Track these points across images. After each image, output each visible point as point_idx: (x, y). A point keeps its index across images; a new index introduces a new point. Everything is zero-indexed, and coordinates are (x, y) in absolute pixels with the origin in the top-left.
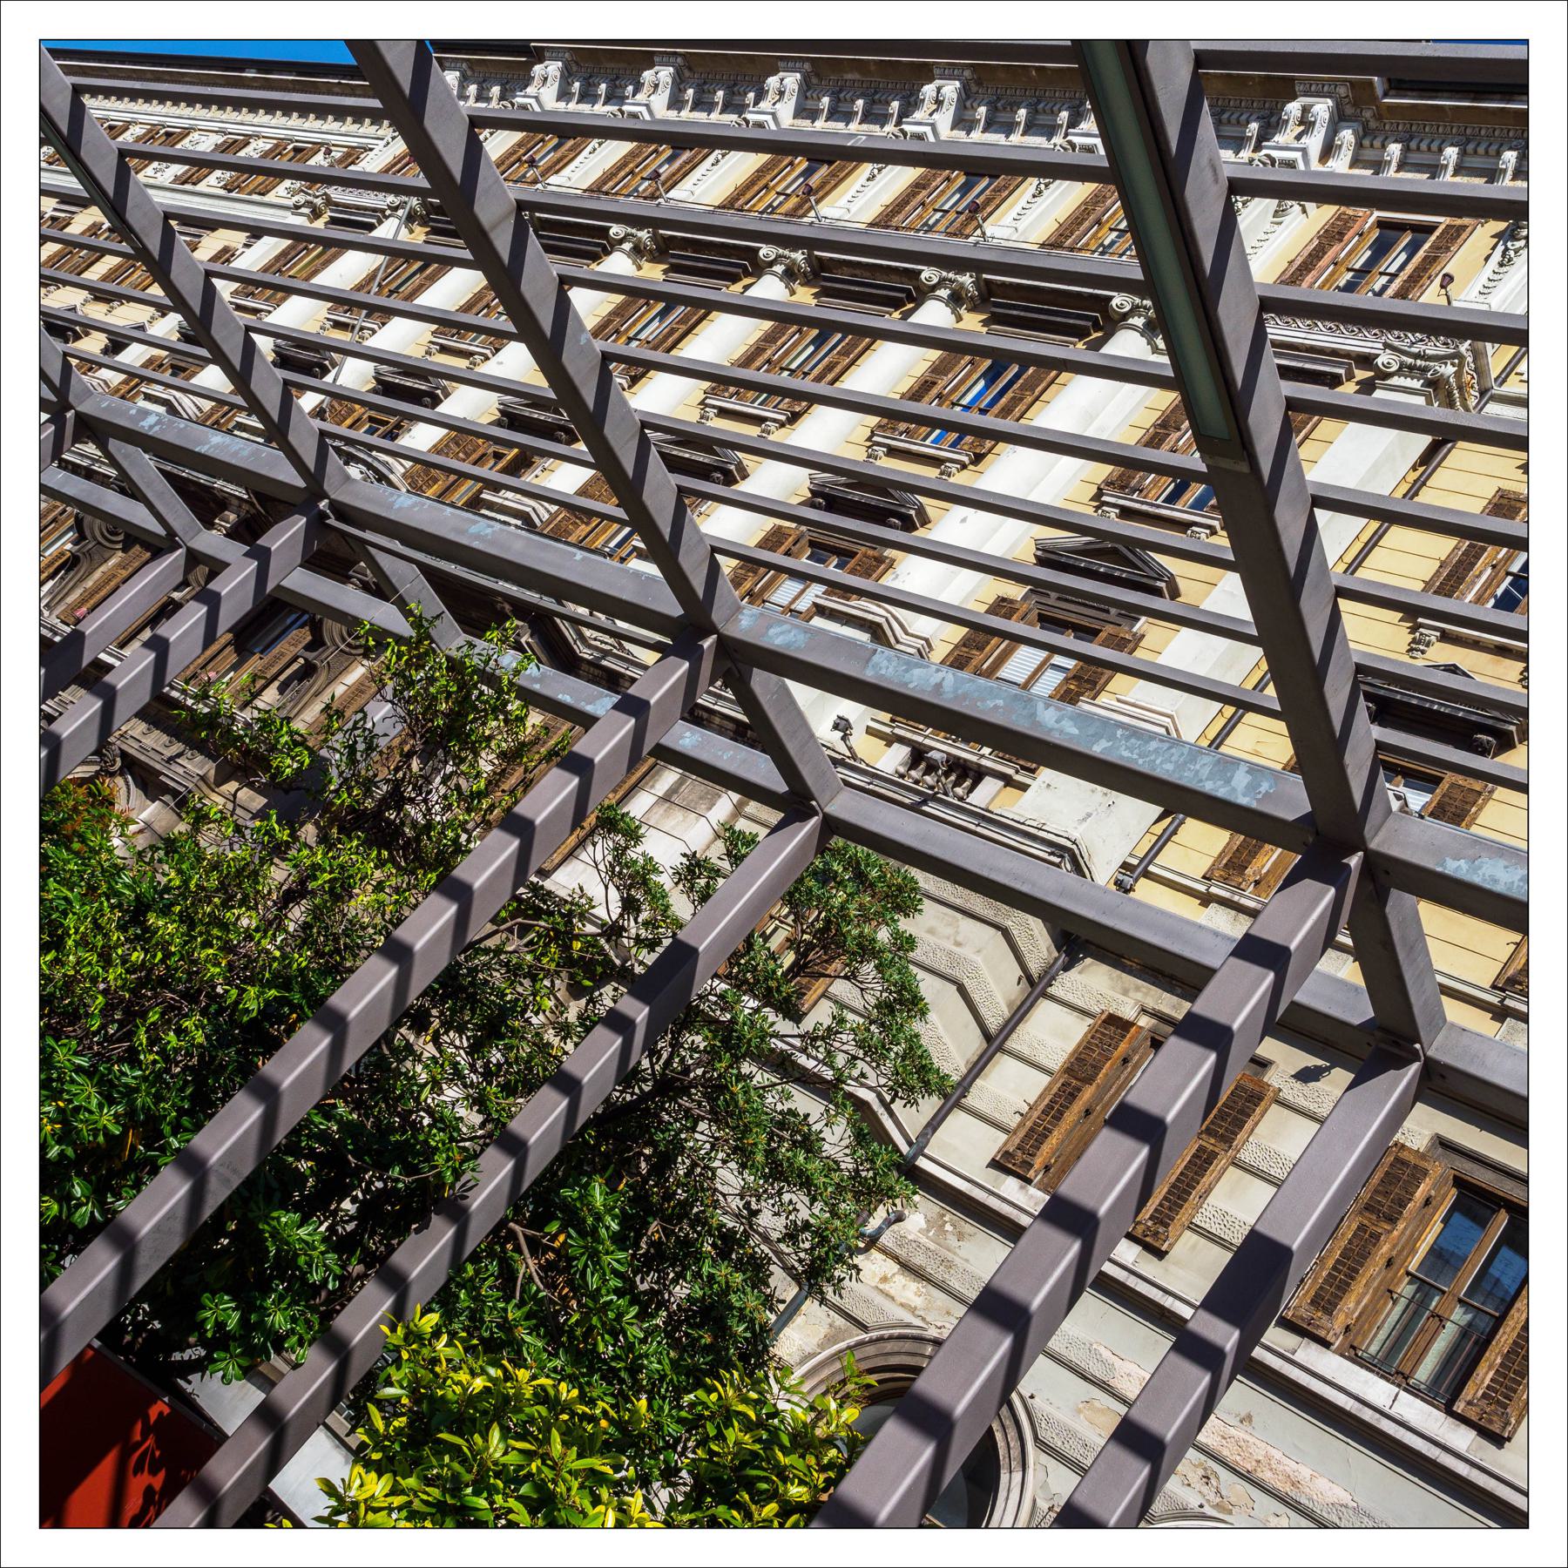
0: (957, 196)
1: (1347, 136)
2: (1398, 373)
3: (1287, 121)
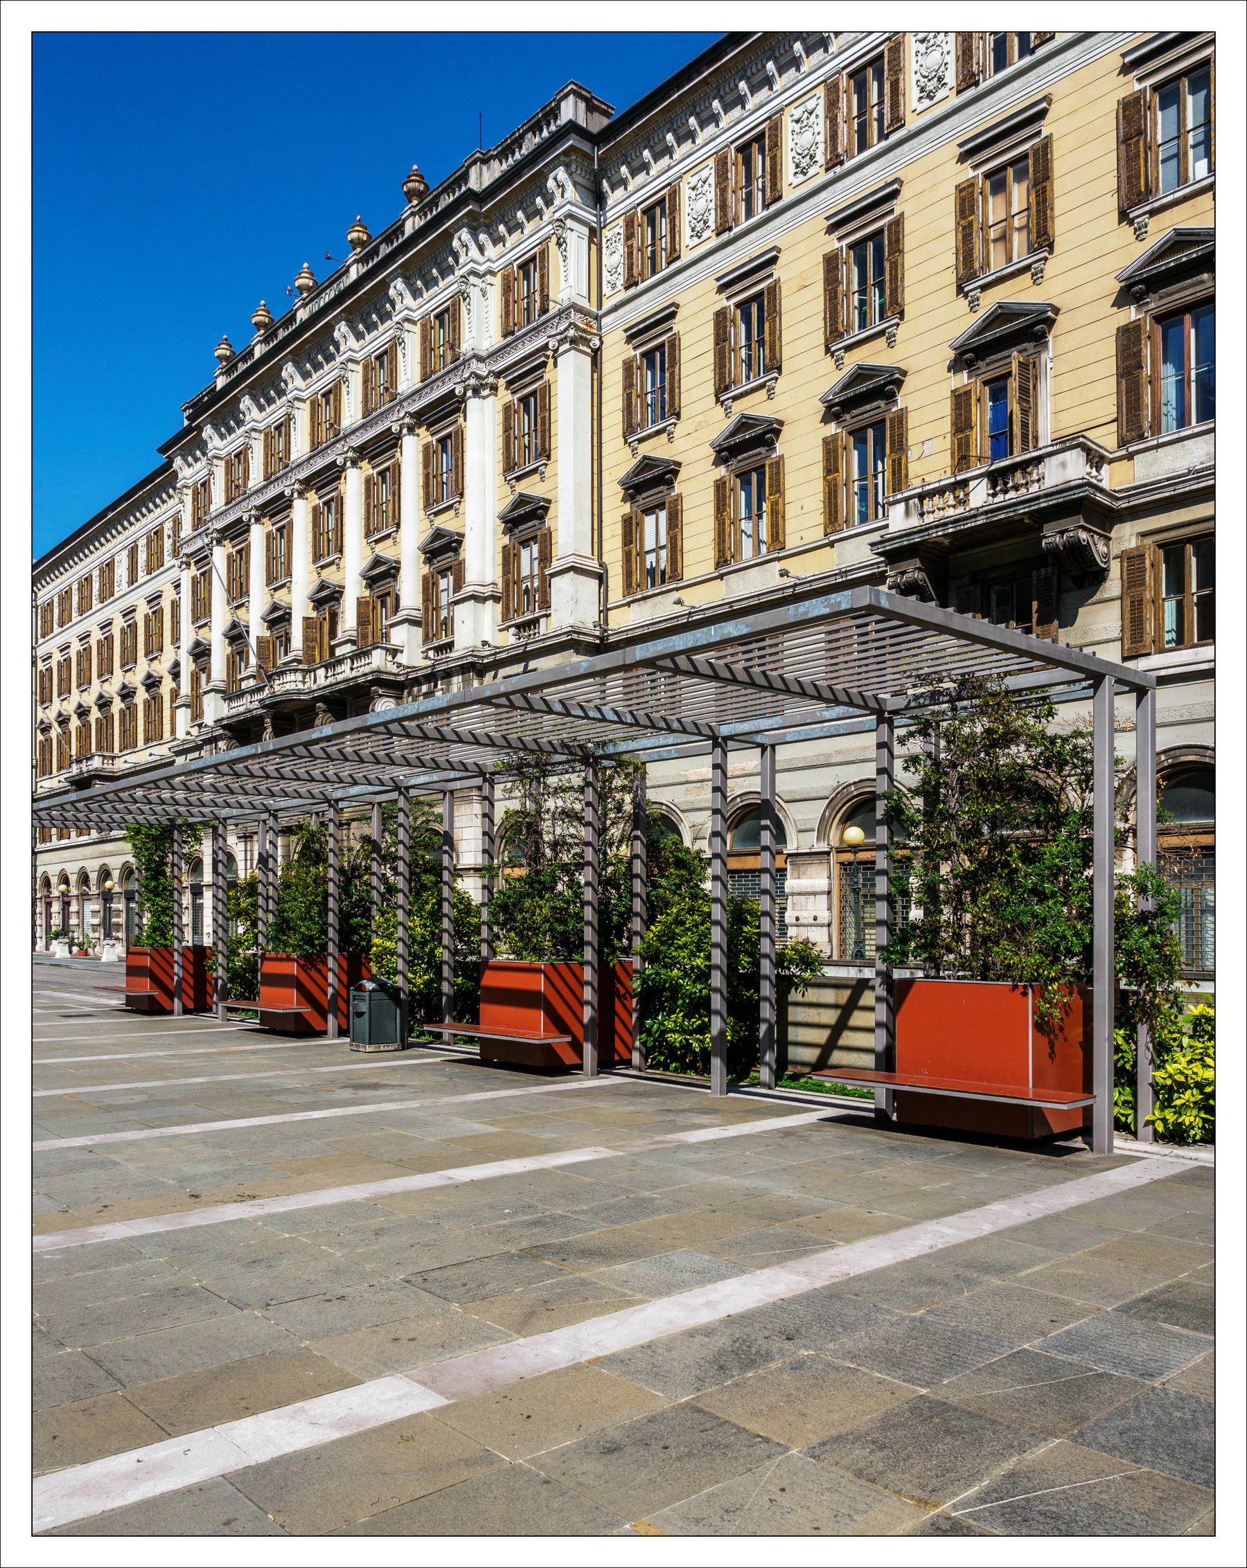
1: (483, 237)
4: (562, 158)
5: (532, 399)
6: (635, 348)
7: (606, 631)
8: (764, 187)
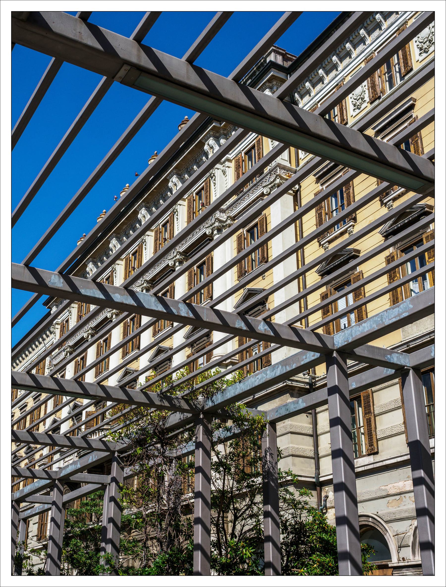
0: (250, 162)
2: (271, 191)
3: (207, 151)
4: (267, 84)
5: (256, 229)
6: (322, 185)
7: (314, 378)
8: (400, 69)
